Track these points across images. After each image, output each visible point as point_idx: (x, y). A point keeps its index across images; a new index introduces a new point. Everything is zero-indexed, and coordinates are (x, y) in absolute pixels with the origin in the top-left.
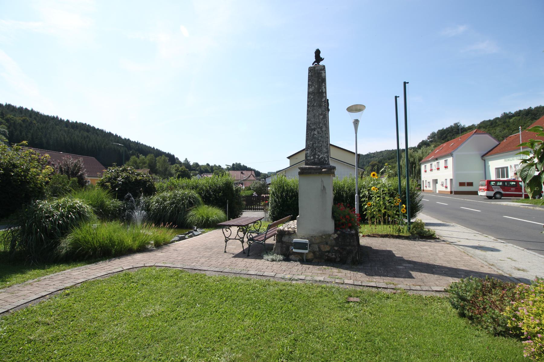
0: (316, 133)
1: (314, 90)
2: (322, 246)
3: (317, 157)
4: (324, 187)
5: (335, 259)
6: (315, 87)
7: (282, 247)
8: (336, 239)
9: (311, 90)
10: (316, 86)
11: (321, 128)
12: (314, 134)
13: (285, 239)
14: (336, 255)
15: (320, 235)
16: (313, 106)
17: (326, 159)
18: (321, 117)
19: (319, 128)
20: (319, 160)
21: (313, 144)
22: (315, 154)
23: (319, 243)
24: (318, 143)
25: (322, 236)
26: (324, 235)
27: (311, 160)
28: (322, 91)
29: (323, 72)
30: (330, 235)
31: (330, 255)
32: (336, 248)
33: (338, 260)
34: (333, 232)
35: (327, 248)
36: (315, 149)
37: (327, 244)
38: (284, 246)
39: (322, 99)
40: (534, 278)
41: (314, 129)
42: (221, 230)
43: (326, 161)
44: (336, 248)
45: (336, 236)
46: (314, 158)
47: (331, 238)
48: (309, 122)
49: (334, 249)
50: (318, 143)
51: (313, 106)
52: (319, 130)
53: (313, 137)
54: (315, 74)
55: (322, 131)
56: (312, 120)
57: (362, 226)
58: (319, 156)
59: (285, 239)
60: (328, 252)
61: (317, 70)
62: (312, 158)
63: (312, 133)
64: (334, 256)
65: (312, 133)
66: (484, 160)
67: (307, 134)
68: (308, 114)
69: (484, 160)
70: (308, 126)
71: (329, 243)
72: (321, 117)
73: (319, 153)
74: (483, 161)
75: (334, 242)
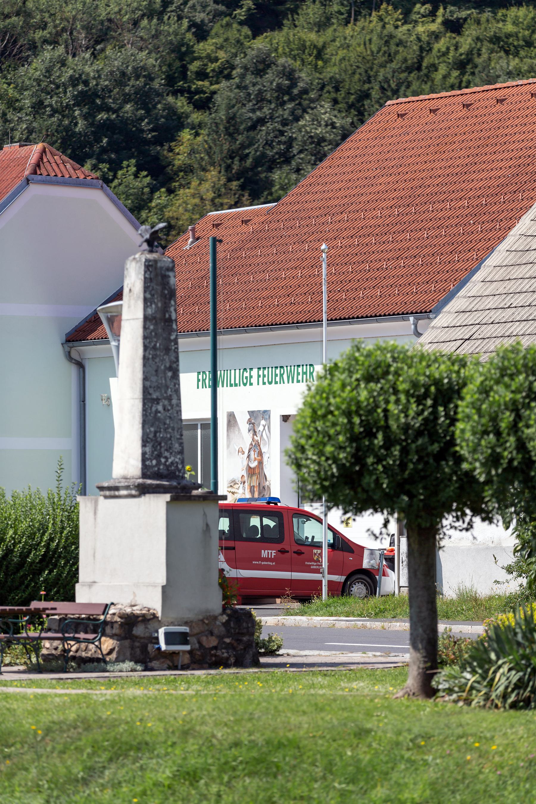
0: (160, 408)
1: (156, 312)
2: (204, 639)
3: (163, 460)
4: (207, 525)
5: (228, 659)
6: (156, 305)
7: (132, 648)
8: (226, 624)
9: (149, 311)
10: (160, 305)
11: (170, 399)
12: (157, 412)
13: (139, 630)
14: (228, 653)
15: (201, 617)
16: (154, 348)
17: (180, 466)
18: (170, 374)
19: (165, 398)
20: (167, 467)
21: (155, 433)
22: (159, 456)
23: (197, 634)
24: (165, 430)
25: (202, 621)
26: (207, 619)
27: (153, 467)
28: (170, 316)
29: (171, 274)
30: (215, 618)
31: (219, 653)
32: (228, 640)
33: (232, 660)
34: (220, 610)
35: (213, 642)
36: (160, 444)
37: (212, 633)
38: (137, 644)
39: (170, 334)
40: (518, 588)
41: (157, 401)
42: (407, 585)
43: (180, 471)
44: (228, 640)
45: (225, 618)
46: (159, 463)
47: (218, 623)
48: (148, 384)
49: (224, 642)
50: (165, 430)
51: (154, 348)
52: (166, 402)
53: (156, 418)
54: (156, 275)
55: (172, 406)
56: (154, 379)
57: (513, 564)
58: (166, 458)
59: (139, 630)
60: (215, 648)
61: (161, 268)
62: (154, 462)
63: (154, 409)
64: (225, 655)
65: (154, 409)
66: (81, 365)
67: (144, 410)
68: (144, 365)
69: (81, 365)
70: (146, 391)
71: (216, 631)
72: (170, 374)
73: (167, 454)
74: (73, 370)
75: (223, 629)
